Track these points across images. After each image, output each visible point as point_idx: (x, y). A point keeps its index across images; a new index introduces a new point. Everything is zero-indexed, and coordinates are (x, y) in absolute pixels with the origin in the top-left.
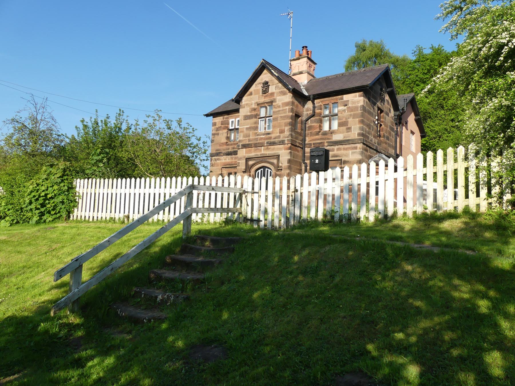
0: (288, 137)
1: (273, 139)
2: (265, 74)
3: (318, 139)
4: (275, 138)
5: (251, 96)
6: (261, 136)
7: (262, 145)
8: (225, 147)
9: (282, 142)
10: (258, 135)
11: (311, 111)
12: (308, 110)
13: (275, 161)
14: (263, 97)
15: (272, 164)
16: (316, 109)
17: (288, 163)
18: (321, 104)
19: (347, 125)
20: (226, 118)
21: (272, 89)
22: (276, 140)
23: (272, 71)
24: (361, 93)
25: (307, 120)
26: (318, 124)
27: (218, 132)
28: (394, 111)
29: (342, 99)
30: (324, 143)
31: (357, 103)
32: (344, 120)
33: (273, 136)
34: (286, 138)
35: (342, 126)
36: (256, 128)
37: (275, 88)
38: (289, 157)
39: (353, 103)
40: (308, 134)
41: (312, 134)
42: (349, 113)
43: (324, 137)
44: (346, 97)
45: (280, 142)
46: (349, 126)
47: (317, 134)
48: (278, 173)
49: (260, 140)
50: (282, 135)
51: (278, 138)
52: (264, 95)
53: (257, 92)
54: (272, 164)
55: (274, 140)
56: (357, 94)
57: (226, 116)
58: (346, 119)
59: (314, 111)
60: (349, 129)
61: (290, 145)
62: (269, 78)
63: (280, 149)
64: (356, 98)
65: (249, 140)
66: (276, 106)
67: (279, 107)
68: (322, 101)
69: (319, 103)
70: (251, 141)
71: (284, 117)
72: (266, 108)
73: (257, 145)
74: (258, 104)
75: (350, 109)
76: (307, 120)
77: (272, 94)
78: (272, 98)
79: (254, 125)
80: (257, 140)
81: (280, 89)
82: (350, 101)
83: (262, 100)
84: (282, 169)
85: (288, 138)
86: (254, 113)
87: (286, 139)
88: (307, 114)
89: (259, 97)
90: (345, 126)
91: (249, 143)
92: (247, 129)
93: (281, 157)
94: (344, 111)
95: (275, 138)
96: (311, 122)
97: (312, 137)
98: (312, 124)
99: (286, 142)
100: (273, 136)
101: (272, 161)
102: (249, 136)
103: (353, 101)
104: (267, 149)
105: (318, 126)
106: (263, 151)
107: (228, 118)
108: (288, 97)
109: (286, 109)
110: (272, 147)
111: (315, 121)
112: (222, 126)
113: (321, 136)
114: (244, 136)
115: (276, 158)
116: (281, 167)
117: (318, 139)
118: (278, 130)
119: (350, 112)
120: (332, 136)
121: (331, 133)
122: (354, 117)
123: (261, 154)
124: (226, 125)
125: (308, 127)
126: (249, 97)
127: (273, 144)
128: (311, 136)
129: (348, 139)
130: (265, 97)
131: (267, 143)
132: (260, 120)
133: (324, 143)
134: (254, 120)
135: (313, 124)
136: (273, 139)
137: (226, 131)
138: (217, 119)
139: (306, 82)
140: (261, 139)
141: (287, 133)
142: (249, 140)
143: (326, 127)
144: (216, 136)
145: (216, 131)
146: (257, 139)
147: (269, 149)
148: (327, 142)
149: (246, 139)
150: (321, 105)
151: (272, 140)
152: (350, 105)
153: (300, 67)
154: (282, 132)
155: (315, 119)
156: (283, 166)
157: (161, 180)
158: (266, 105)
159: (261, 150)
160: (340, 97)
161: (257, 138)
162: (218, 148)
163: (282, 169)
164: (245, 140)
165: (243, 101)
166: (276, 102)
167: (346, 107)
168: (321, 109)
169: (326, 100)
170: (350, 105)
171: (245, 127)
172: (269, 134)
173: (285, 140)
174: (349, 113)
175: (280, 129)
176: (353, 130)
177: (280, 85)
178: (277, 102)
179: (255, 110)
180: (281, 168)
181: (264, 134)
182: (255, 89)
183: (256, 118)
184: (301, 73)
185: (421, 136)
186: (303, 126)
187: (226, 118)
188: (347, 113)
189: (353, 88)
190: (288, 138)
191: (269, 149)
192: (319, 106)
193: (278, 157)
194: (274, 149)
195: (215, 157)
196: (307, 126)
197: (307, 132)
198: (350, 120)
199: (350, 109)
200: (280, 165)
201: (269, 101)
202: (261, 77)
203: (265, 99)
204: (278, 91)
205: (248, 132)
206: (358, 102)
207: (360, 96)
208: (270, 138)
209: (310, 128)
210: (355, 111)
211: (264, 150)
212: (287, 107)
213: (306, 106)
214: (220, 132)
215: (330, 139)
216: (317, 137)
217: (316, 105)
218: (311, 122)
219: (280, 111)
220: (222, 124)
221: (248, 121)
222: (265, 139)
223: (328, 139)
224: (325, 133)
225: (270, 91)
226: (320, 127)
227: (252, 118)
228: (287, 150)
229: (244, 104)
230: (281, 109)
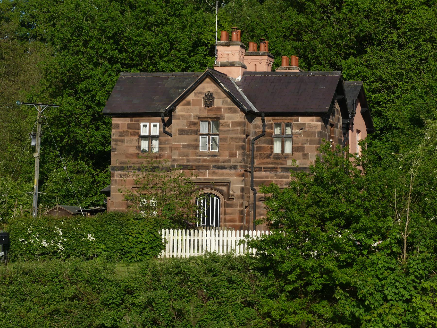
0: (241, 162)
1: (222, 162)
2: (208, 83)
3: (269, 163)
4: (224, 162)
5: (189, 107)
6: (204, 157)
7: (207, 168)
8: (135, 160)
9: (234, 168)
10: (200, 156)
11: (260, 129)
12: (256, 127)
13: (225, 189)
14: (206, 111)
15: (221, 191)
16: (266, 128)
17: (241, 192)
18: (272, 122)
19: (304, 151)
20: (135, 121)
21: (218, 103)
22: (226, 164)
23: (221, 84)
24: (319, 117)
25: (255, 139)
26: (270, 146)
27: (122, 138)
28: (342, 118)
29: (298, 121)
30: (277, 168)
31: (314, 128)
32: (300, 145)
33: (221, 158)
34: (238, 163)
35: (297, 152)
36: (197, 147)
37: (222, 102)
38: (243, 186)
39: (310, 127)
40: (257, 156)
41: (261, 156)
42: (306, 138)
43: (276, 161)
44: (302, 120)
45: (231, 167)
46: (305, 152)
47: (269, 156)
48: (229, 202)
49: (203, 162)
50: (232, 159)
51: (228, 162)
52: (207, 108)
53: (196, 103)
54: (221, 191)
55: (223, 164)
56: (315, 118)
57: (134, 119)
58: (302, 144)
59: (264, 131)
60: (305, 156)
61: (243, 172)
62: (214, 88)
63: (231, 175)
64: (313, 123)
65: (188, 161)
66: (224, 124)
67: (229, 126)
68: (273, 120)
69: (270, 121)
70: (191, 162)
71: (236, 138)
72: (209, 123)
73: (200, 167)
74: (199, 118)
75: (307, 134)
76: (255, 139)
77: (219, 109)
78: (218, 114)
79: (194, 143)
80: (199, 162)
81: (228, 105)
82: (306, 124)
83: (205, 114)
84: (234, 199)
85: (241, 164)
86: (193, 128)
87: (239, 164)
88: (255, 132)
89: (200, 110)
90: (301, 151)
91: (188, 164)
92: (184, 146)
93: (233, 184)
94: (300, 134)
95: (224, 162)
96: (261, 142)
97: (261, 160)
98: (261, 144)
99: (239, 168)
100: (221, 158)
101: (220, 188)
102: (188, 155)
103: (310, 125)
104: (214, 173)
105: (269, 148)
106: (207, 176)
107: (138, 121)
108: (240, 117)
109: (238, 130)
110: (220, 172)
111: (265, 142)
112: (130, 130)
113: (273, 160)
114: (180, 155)
115: (225, 185)
116: (233, 195)
117: (269, 163)
118: (227, 153)
119: (307, 137)
120: (286, 161)
121: (285, 158)
122: (311, 142)
123: (205, 179)
124: (137, 131)
125: (257, 147)
126: (186, 107)
127: (223, 168)
128: (260, 158)
129: (304, 166)
130: (209, 111)
131: (214, 167)
132: (200, 136)
133: (277, 168)
134: (193, 137)
135: (263, 145)
136: (222, 162)
137: (136, 138)
138: (121, 120)
139: (239, 78)
140: (205, 160)
141: (239, 157)
142: (187, 160)
143: (277, 148)
144: (119, 143)
145: (120, 136)
146: (199, 161)
147: (217, 173)
148: (280, 168)
149: (183, 159)
150: (272, 124)
151: (220, 164)
152: (306, 129)
153: (230, 56)
154: (233, 155)
155: (265, 140)
156: (235, 194)
157: (194, 232)
158: (210, 120)
159: (205, 174)
160: (295, 118)
161: (199, 159)
162: (124, 159)
163: (234, 199)
164: (181, 159)
165: (177, 110)
166: (224, 119)
167: (302, 131)
168: (272, 128)
169: (279, 119)
170: (306, 129)
171: (181, 143)
172: (215, 156)
173: (237, 166)
174: (306, 138)
175: (229, 152)
176: (310, 158)
177: (229, 100)
178: (225, 120)
179: (195, 124)
180: (233, 197)
181: (209, 156)
182: (194, 98)
183: (197, 134)
184: (232, 64)
185: (367, 131)
186: (251, 146)
187: (135, 121)
188: (302, 138)
189: (312, 112)
190: (241, 164)
191: (217, 173)
192: (270, 124)
193: (228, 184)
194: (222, 174)
195: (119, 172)
196: (255, 146)
197: (255, 153)
198: (307, 146)
199: (307, 134)
200: (231, 193)
201: (215, 116)
202: (201, 85)
203: (209, 114)
204: (226, 106)
205: (185, 150)
206: (316, 127)
207: (318, 121)
208: (218, 161)
209: (259, 149)
210: (312, 137)
211: (209, 174)
212: (239, 128)
213: (253, 122)
214: (126, 138)
215: (283, 164)
216: (268, 160)
217: (266, 123)
218: (261, 142)
219: (229, 130)
220: (129, 128)
221: (185, 136)
222: (209, 161)
223: (282, 164)
224: (277, 157)
225: (215, 105)
226: (272, 149)
227: (191, 134)
228: (240, 177)
229: (179, 115)
230: (231, 128)
